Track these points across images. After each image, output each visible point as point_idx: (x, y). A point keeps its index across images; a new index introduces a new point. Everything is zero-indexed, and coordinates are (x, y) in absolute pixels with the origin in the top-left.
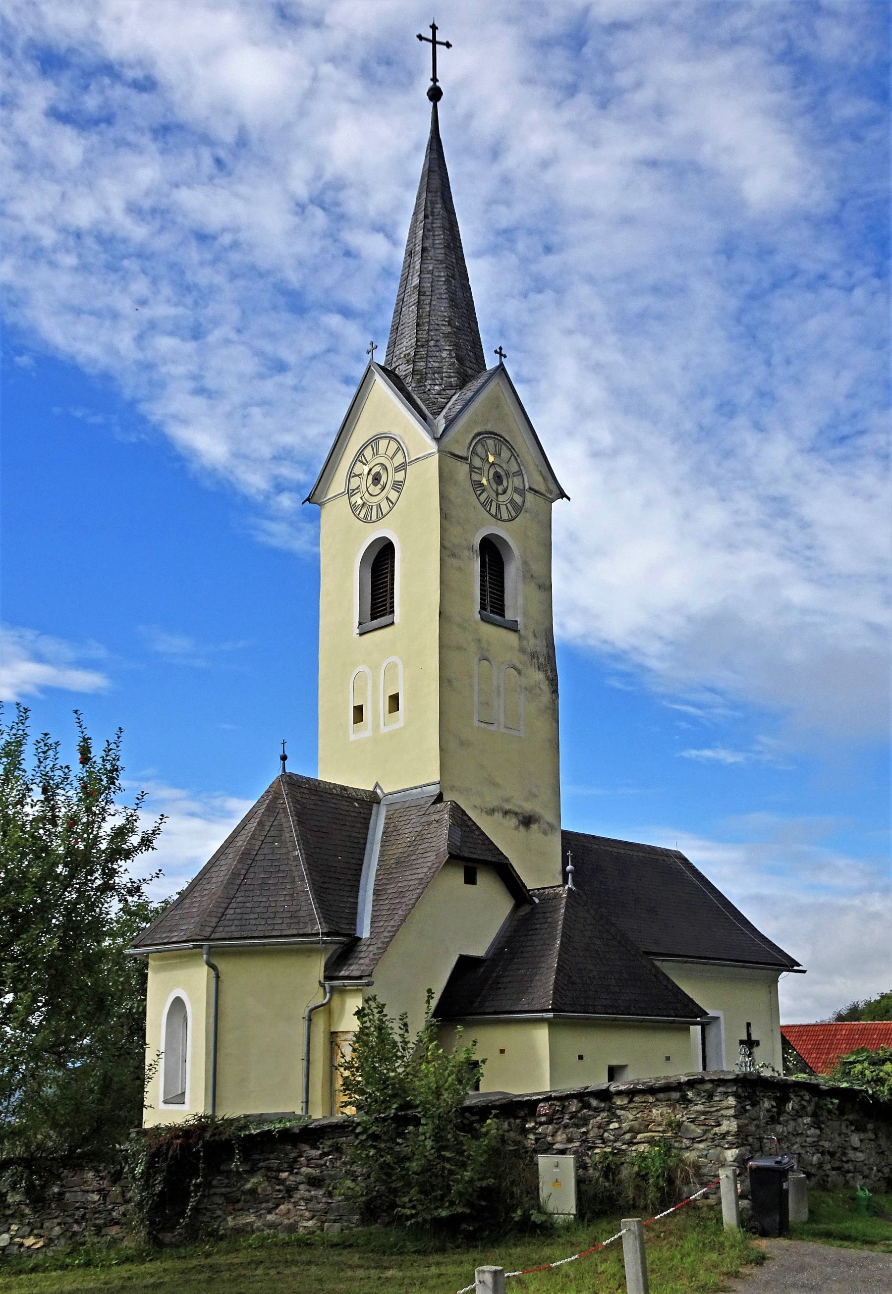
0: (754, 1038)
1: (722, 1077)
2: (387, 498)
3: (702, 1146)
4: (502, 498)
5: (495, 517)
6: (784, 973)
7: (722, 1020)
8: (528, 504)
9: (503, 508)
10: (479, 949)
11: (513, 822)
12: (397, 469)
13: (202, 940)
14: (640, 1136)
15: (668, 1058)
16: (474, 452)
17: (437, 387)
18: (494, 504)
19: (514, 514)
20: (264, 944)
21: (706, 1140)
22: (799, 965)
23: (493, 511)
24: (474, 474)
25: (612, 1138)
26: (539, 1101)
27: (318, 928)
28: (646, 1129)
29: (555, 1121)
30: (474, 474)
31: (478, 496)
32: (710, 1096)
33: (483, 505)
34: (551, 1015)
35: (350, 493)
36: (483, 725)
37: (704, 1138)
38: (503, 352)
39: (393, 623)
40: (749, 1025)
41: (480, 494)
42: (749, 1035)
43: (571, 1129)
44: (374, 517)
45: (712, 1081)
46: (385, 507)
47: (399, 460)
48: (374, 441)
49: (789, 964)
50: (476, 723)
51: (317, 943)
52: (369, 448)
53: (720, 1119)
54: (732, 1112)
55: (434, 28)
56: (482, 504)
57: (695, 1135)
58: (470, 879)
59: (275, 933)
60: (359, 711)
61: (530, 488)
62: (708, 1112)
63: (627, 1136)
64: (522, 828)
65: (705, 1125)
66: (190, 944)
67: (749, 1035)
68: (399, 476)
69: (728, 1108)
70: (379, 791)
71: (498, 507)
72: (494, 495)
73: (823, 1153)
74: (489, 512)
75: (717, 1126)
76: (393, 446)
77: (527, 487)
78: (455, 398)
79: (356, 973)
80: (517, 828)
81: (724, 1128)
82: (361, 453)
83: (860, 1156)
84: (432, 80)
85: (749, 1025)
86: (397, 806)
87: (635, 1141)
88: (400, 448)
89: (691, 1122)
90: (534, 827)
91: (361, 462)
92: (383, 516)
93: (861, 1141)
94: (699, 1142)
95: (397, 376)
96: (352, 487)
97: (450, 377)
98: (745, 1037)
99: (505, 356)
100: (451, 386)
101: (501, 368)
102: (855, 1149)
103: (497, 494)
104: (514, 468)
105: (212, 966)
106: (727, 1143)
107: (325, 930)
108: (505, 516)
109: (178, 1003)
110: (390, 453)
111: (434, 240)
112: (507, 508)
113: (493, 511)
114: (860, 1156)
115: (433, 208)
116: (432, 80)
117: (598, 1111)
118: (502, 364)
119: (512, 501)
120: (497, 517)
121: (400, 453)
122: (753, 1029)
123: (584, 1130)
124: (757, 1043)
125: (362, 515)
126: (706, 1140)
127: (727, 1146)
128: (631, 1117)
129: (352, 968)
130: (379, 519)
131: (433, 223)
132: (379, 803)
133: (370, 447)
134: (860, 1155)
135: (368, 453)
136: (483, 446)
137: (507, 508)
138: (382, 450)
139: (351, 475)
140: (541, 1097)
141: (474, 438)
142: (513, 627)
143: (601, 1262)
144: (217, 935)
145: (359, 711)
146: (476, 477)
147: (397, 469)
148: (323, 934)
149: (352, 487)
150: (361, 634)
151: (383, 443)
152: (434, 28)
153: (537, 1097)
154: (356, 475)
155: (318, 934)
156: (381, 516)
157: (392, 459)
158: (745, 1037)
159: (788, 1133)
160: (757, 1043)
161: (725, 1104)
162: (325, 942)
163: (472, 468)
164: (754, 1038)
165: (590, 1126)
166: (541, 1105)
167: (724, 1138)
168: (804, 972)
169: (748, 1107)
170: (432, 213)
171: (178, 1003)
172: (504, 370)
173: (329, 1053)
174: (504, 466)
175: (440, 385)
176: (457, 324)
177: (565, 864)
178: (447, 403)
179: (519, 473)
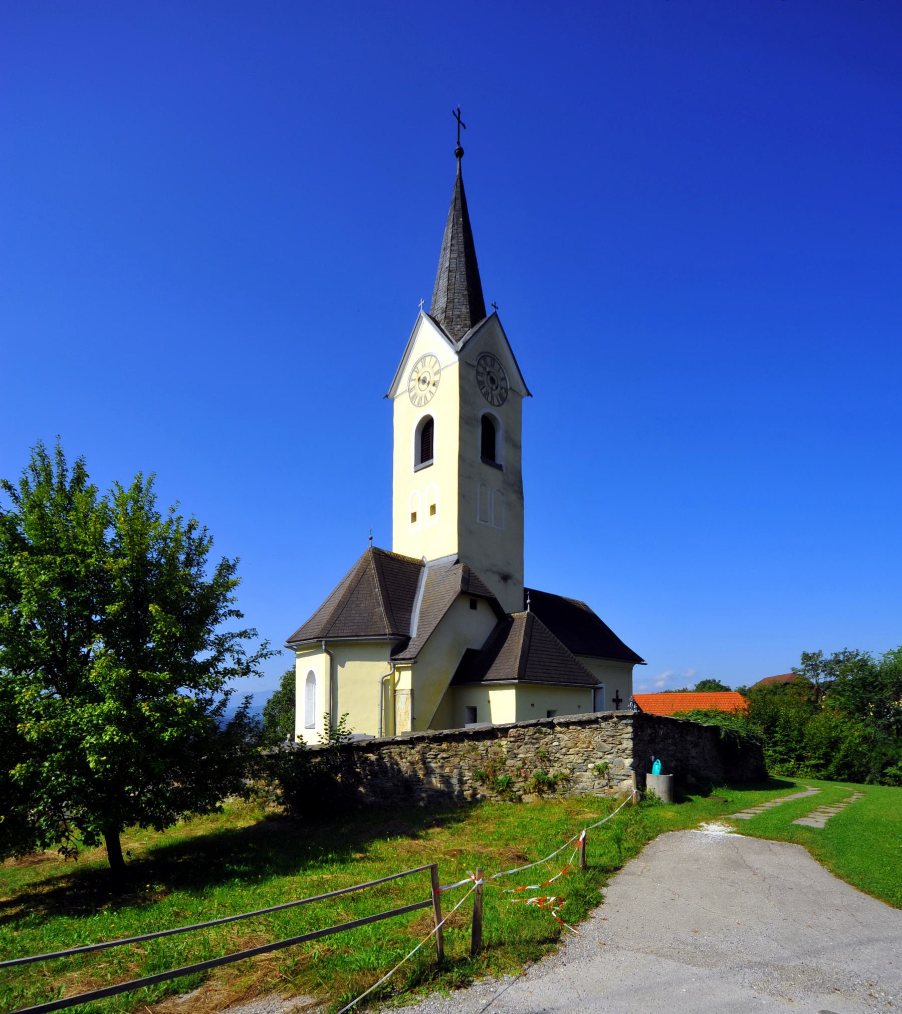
0: (620, 698)
1: (624, 714)
2: (430, 392)
3: (609, 756)
4: (494, 392)
5: (491, 403)
6: (636, 665)
7: (604, 688)
8: (509, 397)
9: (495, 398)
10: (477, 646)
12: (436, 374)
13: (322, 638)
14: (571, 750)
15: (579, 707)
16: (479, 363)
17: (459, 326)
18: (490, 396)
19: (501, 403)
20: (357, 640)
21: (613, 753)
22: (644, 661)
23: (489, 399)
24: (479, 377)
25: (554, 751)
26: (510, 728)
27: (387, 631)
28: (576, 745)
29: (216, 670)
30: (479, 377)
31: (481, 390)
33: (484, 395)
34: (517, 681)
35: (410, 390)
36: (483, 523)
37: (612, 752)
38: (496, 305)
39: (432, 464)
40: (617, 691)
41: (482, 389)
42: (617, 696)
43: (529, 746)
44: (423, 403)
45: (617, 717)
46: (429, 397)
47: (437, 368)
48: (423, 358)
49: (639, 660)
50: (478, 521)
51: (386, 639)
52: (420, 363)
53: (622, 740)
54: (629, 735)
56: (483, 395)
57: (606, 750)
58: (473, 606)
59: (362, 634)
60: (414, 516)
61: (511, 388)
62: (614, 736)
63: (564, 750)
64: (502, 582)
65: (612, 744)
66: (315, 640)
67: (617, 696)
68: (437, 378)
69: (627, 733)
70: (424, 560)
72: (490, 390)
73: (677, 761)
74: (487, 400)
75: (619, 745)
76: (434, 360)
77: (509, 387)
78: (468, 332)
79: (408, 657)
81: (624, 746)
82: (415, 366)
83: (696, 762)
85: (617, 691)
86: (435, 567)
87: (568, 753)
88: (437, 361)
89: (604, 742)
90: (509, 582)
91: (416, 371)
92: (428, 402)
93: (696, 753)
94: (608, 754)
95: (436, 320)
96: (411, 387)
97: (466, 320)
98: (615, 697)
99: (497, 308)
100: (465, 326)
101: (495, 314)
102: (693, 757)
103: (492, 390)
106: (626, 755)
107: (391, 632)
108: (496, 403)
110: (432, 365)
111: (458, 239)
113: (489, 399)
114: (696, 762)
115: (457, 221)
117: (546, 734)
118: (495, 312)
119: (500, 395)
120: (492, 403)
121: (437, 363)
122: (619, 693)
123: (537, 746)
124: (621, 700)
125: (416, 403)
126: (613, 753)
127: (625, 757)
128: (566, 738)
129: (406, 654)
130: (425, 404)
131: (457, 230)
132: (424, 566)
133: (420, 363)
134: (696, 761)
135: (420, 365)
136: (484, 360)
138: (427, 363)
139: (410, 380)
140: (511, 726)
141: (479, 355)
142: (499, 467)
144: (330, 635)
145: (414, 516)
146: (480, 378)
147: (436, 374)
148: (389, 634)
149: (411, 387)
150: (415, 472)
151: (428, 359)
153: (508, 726)
154: (413, 380)
155: (386, 635)
156: (426, 402)
157: (433, 367)
158: (615, 697)
159: (660, 749)
160: (621, 700)
161: (626, 731)
162: (390, 639)
163: (478, 373)
164: (620, 698)
165: (541, 744)
166: (511, 730)
167: (624, 752)
168: (646, 664)
169: (639, 733)
170: (457, 224)
172: (497, 316)
174: (496, 373)
175: (460, 325)
177: (526, 599)
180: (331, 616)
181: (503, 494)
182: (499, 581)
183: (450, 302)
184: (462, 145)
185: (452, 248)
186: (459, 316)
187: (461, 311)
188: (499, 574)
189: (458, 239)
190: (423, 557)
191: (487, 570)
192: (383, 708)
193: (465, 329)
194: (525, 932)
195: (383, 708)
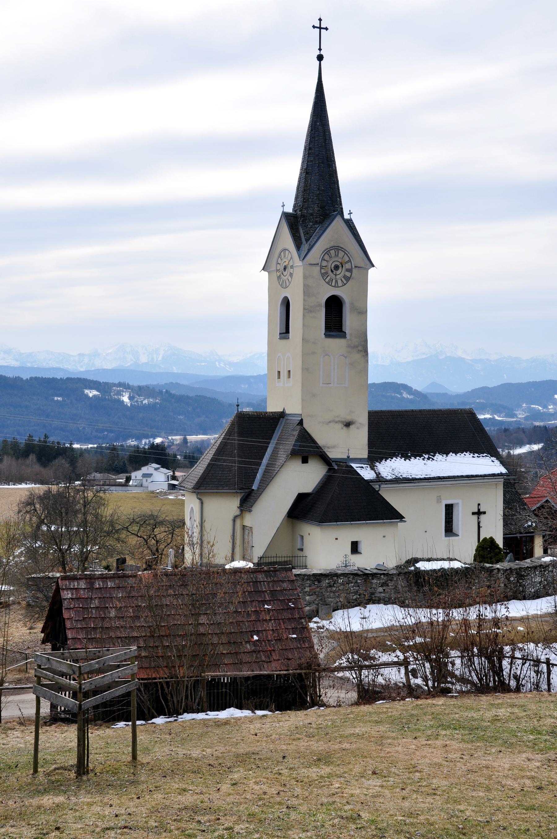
7: (460, 505)
11: (340, 425)
18: (334, 281)
19: (345, 282)
32: (303, 580)
33: (328, 283)
36: (325, 385)
50: (321, 385)
55: (320, 20)
64: (345, 428)
71: (336, 281)
80: (342, 428)
81: (306, 590)
84: (319, 49)
85: (479, 505)
90: (352, 427)
97: (316, 218)
104: (347, 259)
105: (200, 499)
109: (192, 509)
111: (315, 143)
112: (342, 280)
116: (319, 49)
137: (342, 280)
143: (482, 602)
152: (320, 20)
158: (476, 510)
161: (307, 582)
164: (475, 517)
171: (192, 509)
173: (242, 531)
176: (323, 188)
178: (314, 233)
179: (350, 261)
180: (231, 425)
181: (346, 357)
182: (342, 428)
183: (305, 202)
184: (318, 62)
185: (310, 151)
186: (312, 215)
187: (313, 210)
188: (342, 422)
189: (315, 143)
190: (284, 409)
191: (330, 422)
192: (86, 740)
193: (316, 226)
194: (106, 750)
195: (86, 740)
